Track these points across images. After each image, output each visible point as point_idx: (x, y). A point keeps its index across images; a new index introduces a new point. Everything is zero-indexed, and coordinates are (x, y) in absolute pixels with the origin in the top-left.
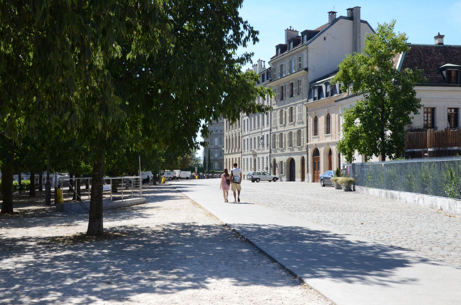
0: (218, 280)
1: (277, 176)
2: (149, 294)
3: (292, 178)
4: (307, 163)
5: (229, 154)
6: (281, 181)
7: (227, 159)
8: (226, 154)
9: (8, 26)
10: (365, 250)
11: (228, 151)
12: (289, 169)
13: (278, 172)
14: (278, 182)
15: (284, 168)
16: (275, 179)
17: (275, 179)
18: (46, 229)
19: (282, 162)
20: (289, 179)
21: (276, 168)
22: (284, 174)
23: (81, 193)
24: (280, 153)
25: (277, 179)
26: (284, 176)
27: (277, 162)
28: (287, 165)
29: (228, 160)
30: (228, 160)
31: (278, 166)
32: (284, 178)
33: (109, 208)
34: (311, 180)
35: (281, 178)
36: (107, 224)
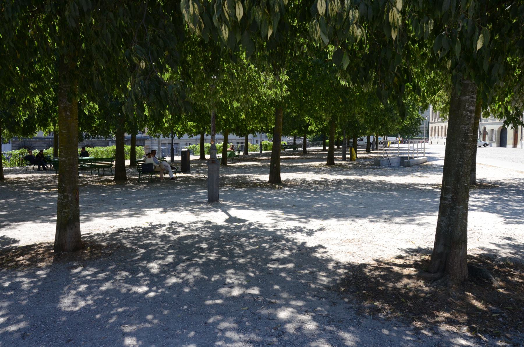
0: (346, 220)
1: (487, 142)
2: (360, 219)
3: (502, 143)
4: (521, 131)
5: (435, 123)
6: (491, 146)
7: (432, 127)
8: (432, 123)
9: (432, 76)
10: (424, 212)
11: (433, 120)
12: (499, 137)
13: (488, 139)
14: (488, 148)
15: (494, 135)
16: (486, 145)
17: (486, 145)
18: (402, 178)
19: (492, 130)
20: (499, 145)
21: (486, 135)
22: (494, 140)
23: (335, 156)
24: (491, 122)
25: (487, 145)
26: (494, 142)
27: (487, 130)
28: (498, 133)
29: (434, 128)
30: (434, 128)
31: (489, 133)
32: (494, 145)
33: (433, 169)
34: (512, 146)
35: (490, 144)
36: (284, 177)
